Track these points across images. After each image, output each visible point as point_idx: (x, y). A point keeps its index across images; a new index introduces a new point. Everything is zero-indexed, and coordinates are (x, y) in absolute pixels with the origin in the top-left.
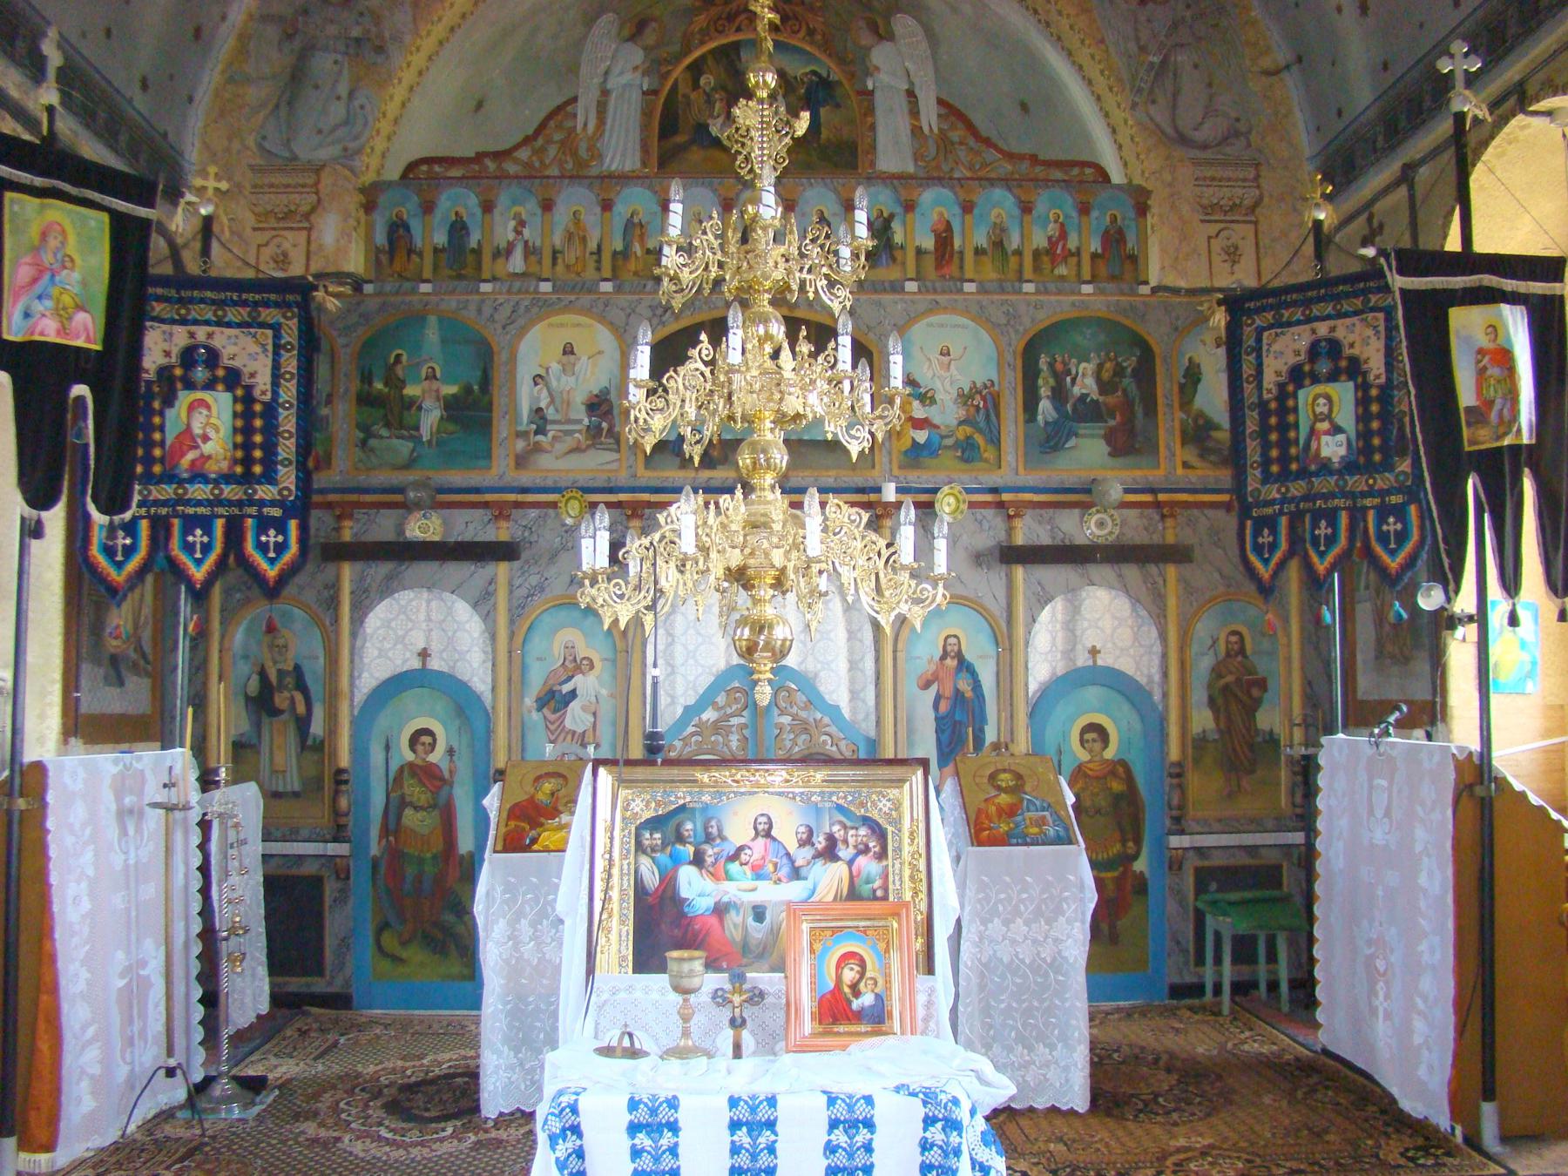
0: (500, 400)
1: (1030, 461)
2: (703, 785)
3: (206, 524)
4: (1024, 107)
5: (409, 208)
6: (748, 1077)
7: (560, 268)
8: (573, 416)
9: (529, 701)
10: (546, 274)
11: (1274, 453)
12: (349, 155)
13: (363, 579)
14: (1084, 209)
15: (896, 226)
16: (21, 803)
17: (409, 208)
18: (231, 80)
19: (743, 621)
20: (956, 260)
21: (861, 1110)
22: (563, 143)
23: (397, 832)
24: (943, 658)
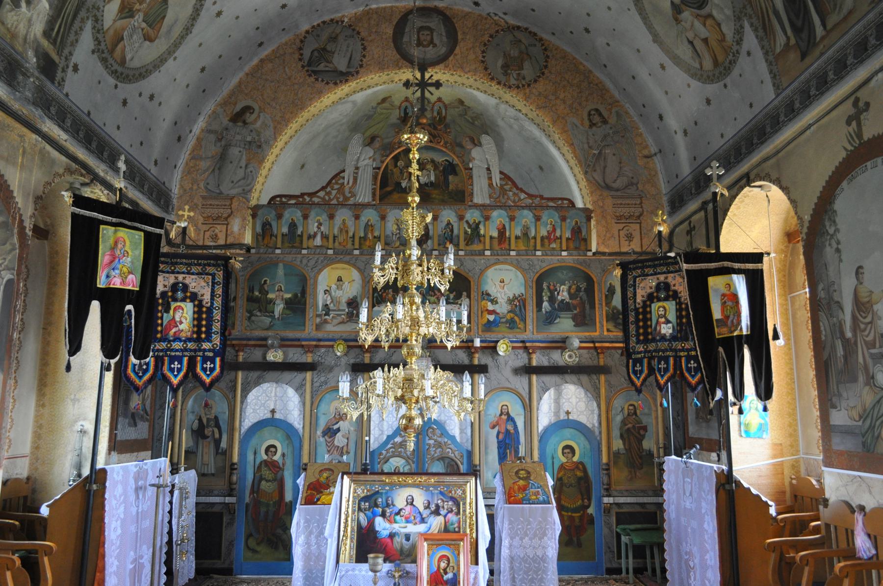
0: (309, 300)
4: (541, 168)
7: (337, 244)
8: (341, 308)
9: (319, 433)
10: (330, 246)
11: (641, 331)
13: (247, 378)
14: (563, 219)
15: (481, 227)
16: (95, 487)
17: (271, 216)
24: (501, 415)
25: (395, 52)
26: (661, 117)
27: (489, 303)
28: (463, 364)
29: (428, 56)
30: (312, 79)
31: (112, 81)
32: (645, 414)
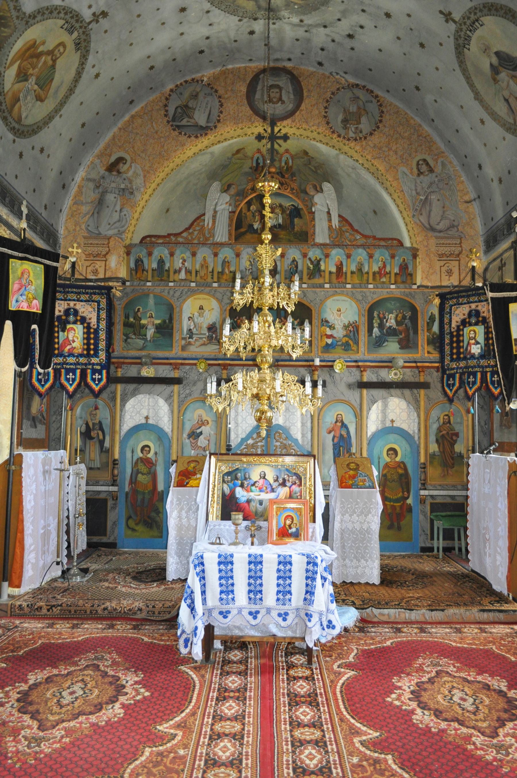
0: (175, 326)
1: (369, 351)
3: (74, 372)
4: (375, 212)
5: (143, 254)
6: (256, 550)
7: (198, 277)
9: (185, 435)
11: (455, 351)
12: (120, 233)
13: (125, 390)
14: (393, 257)
15: (322, 263)
16: (13, 467)
17: (143, 254)
18: (75, 203)
19: (257, 411)
20: (344, 276)
23: (135, 483)
24: (336, 422)
25: (248, 108)
26: (480, 167)
27: (328, 329)
28: (306, 369)
29: (277, 112)
30: (176, 133)
31: (11, 136)
32: (458, 423)
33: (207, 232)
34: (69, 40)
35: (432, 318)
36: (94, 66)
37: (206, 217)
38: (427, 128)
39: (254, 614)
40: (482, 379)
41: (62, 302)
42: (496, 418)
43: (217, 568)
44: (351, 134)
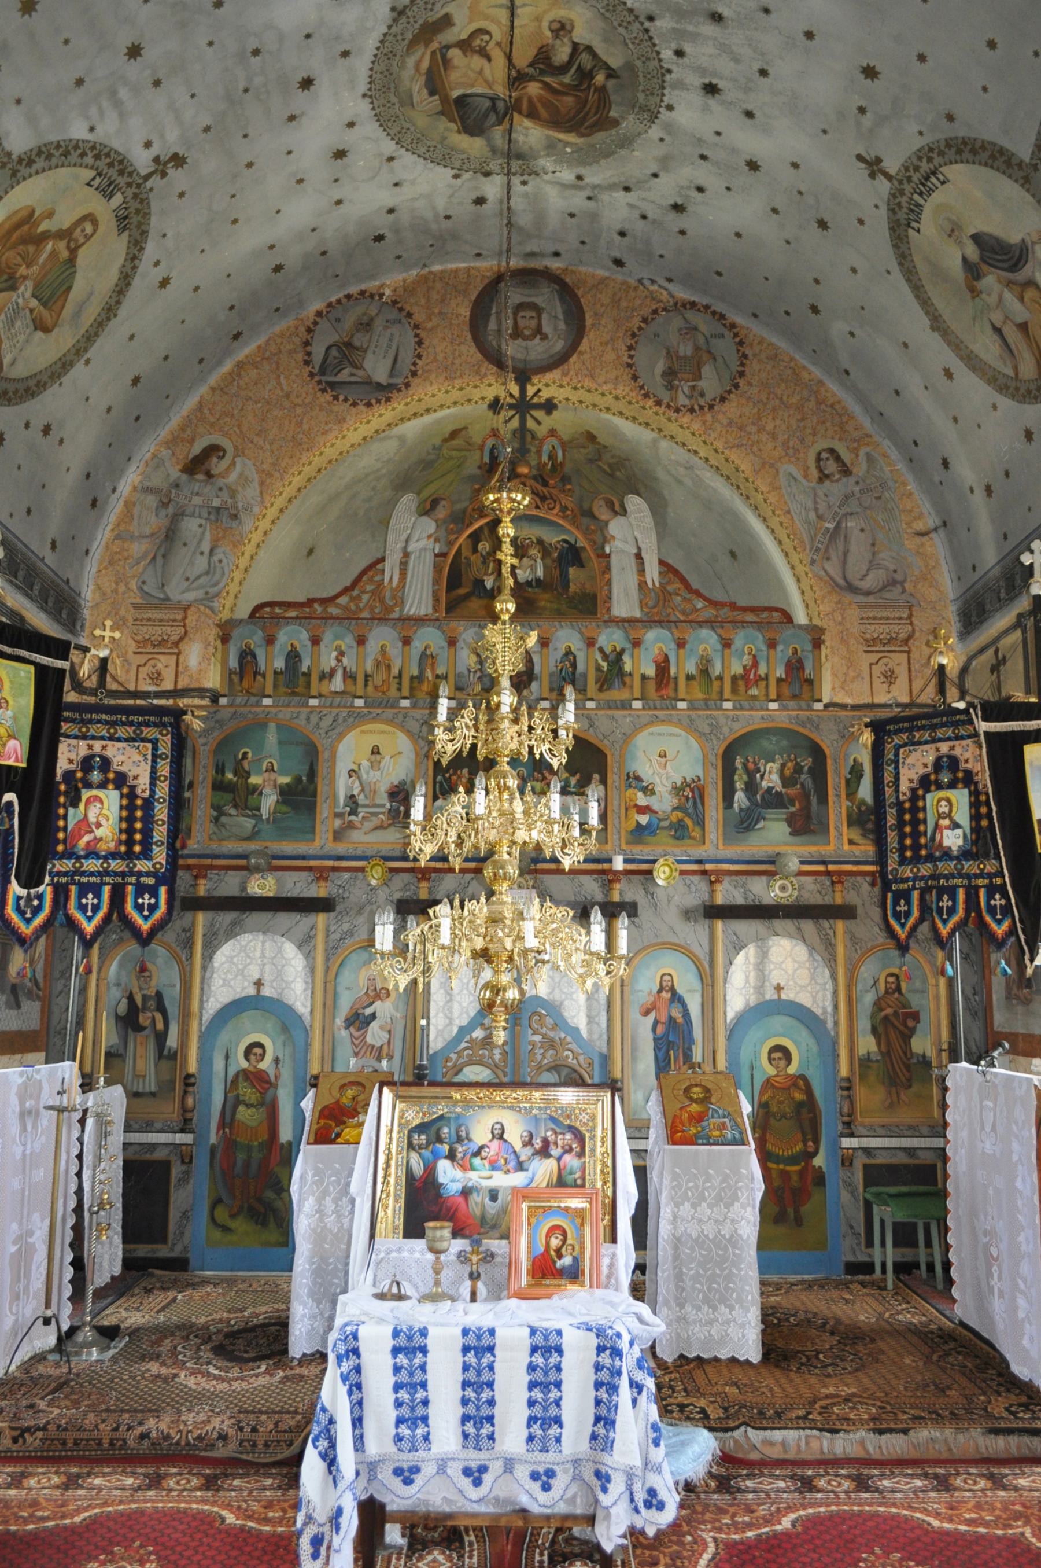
0: (322, 788)
1: (728, 840)
2: (456, 1102)
4: (733, 554)
5: (255, 639)
6: (480, 1315)
7: (370, 688)
9: (339, 1021)
12: (209, 598)
13: (212, 925)
14: (772, 644)
15: (626, 658)
17: (255, 639)
18: (118, 537)
20: (672, 685)
21: (553, 1340)
22: (373, 592)
24: (660, 991)
25: (473, 349)
26: (946, 464)
27: (640, 794)
30: (328, 397)
32: (917, 991)
33: (388, 594)
34: (105, 209)
35: (856, 772)
36: (157, 264)
37: (387, 565)
38: (833, 387)
39: (475, 1475)
40: (967, 901)
41: (74, 742)
42: (998, 985)
43: (388, 1361)
44: (682, 400)
